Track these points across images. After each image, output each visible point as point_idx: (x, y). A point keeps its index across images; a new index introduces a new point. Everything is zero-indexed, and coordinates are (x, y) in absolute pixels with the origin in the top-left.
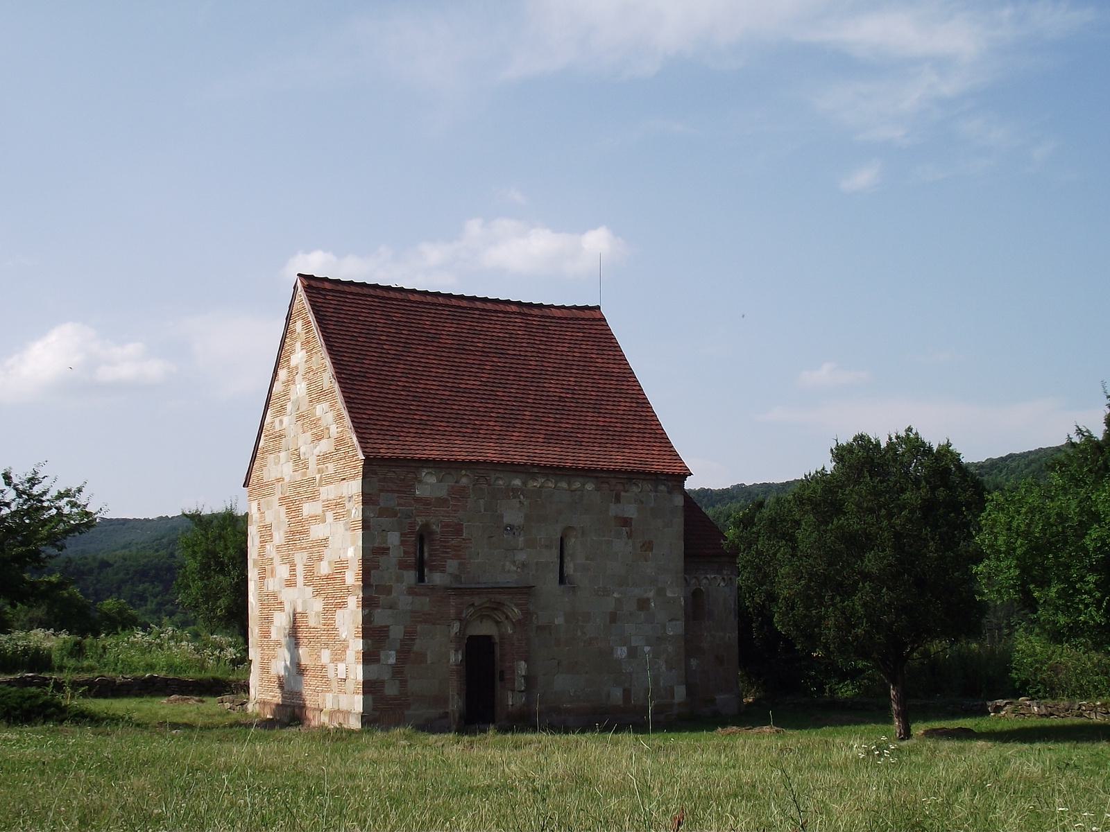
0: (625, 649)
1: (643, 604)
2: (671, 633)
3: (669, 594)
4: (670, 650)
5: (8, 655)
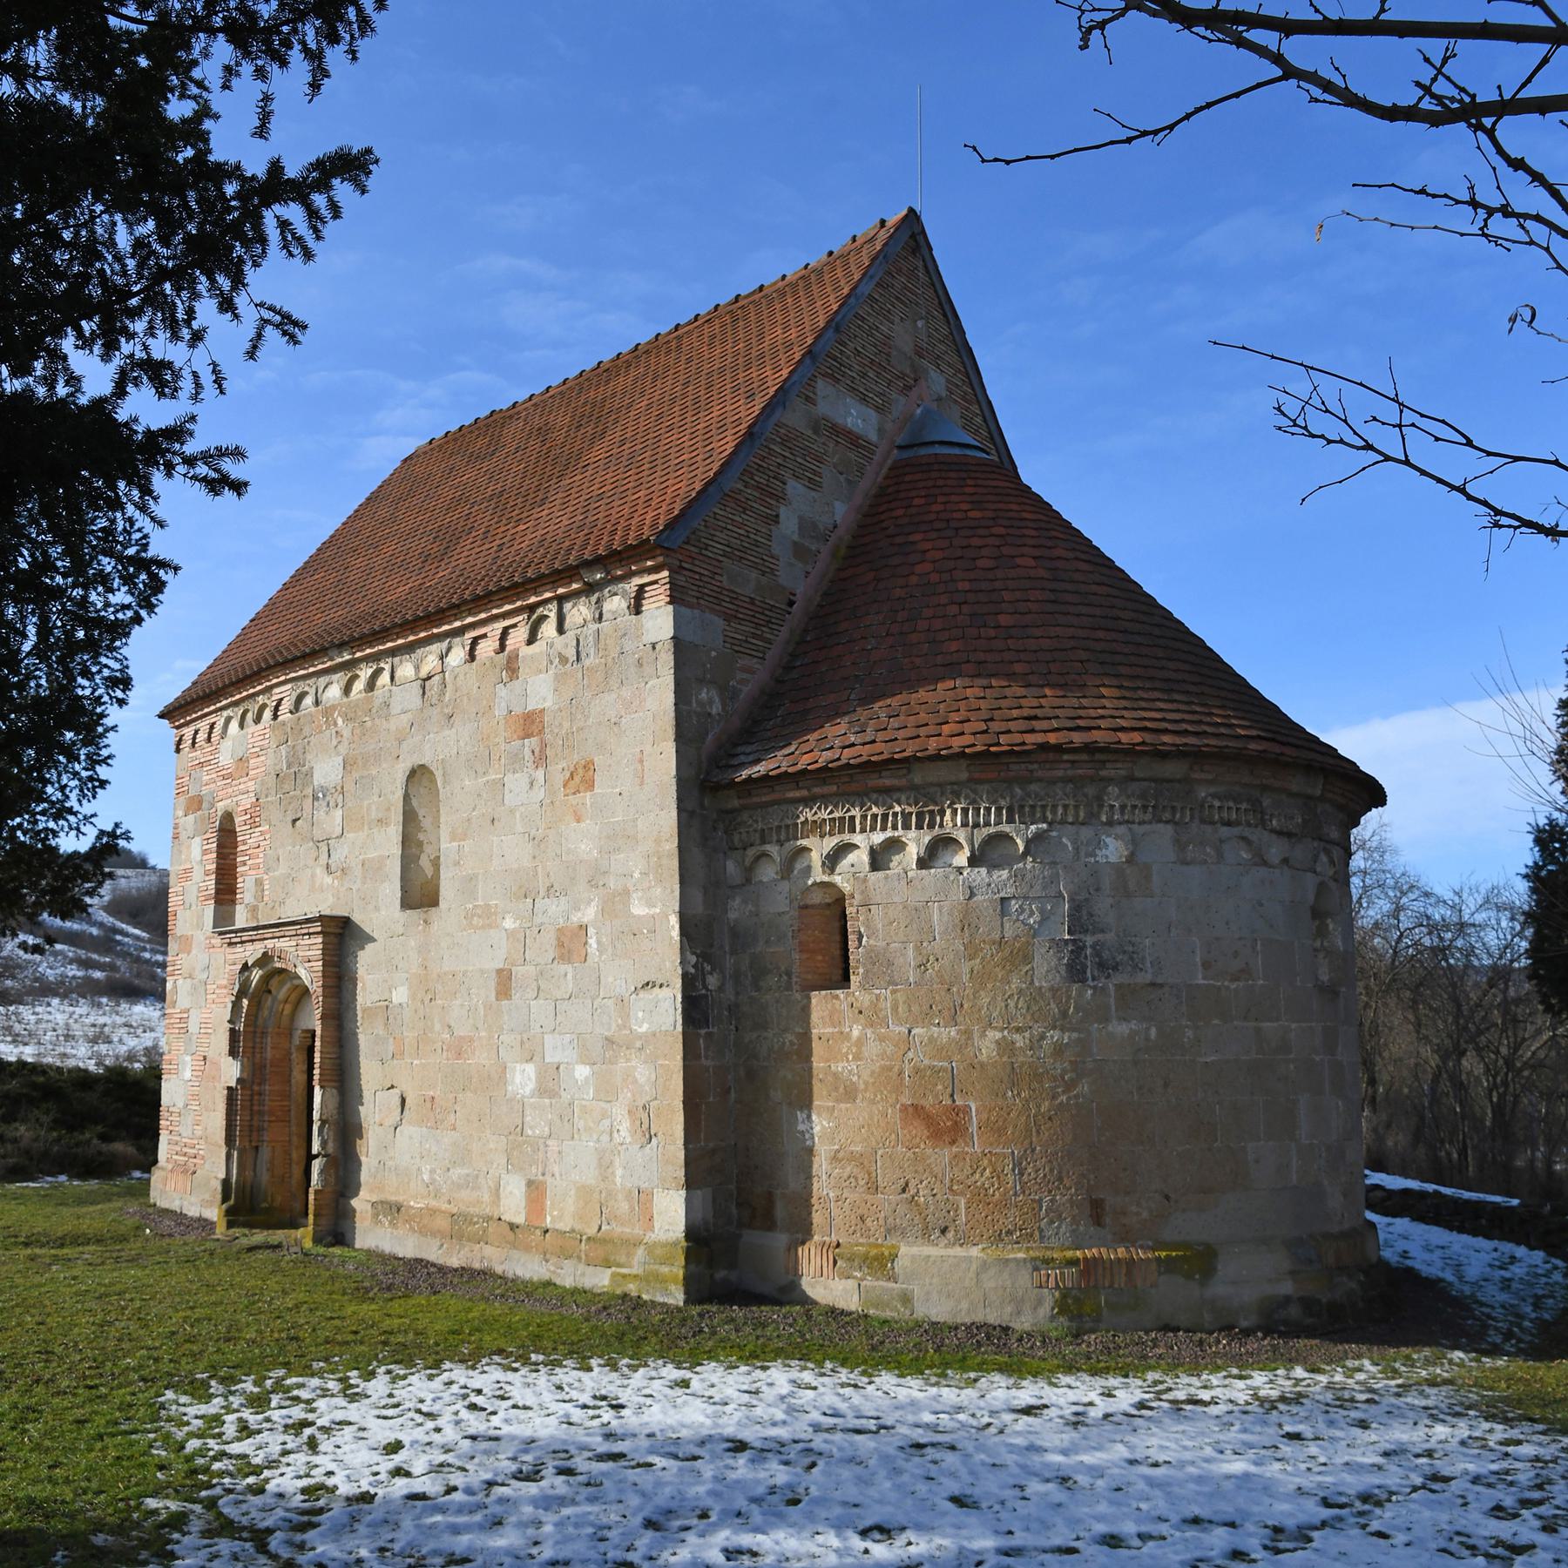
0: (530, 1069)
1: (570, 943)
2: (644, 1028)
3: (638, 909)
4: (642, 1080)
5: (113, 21)
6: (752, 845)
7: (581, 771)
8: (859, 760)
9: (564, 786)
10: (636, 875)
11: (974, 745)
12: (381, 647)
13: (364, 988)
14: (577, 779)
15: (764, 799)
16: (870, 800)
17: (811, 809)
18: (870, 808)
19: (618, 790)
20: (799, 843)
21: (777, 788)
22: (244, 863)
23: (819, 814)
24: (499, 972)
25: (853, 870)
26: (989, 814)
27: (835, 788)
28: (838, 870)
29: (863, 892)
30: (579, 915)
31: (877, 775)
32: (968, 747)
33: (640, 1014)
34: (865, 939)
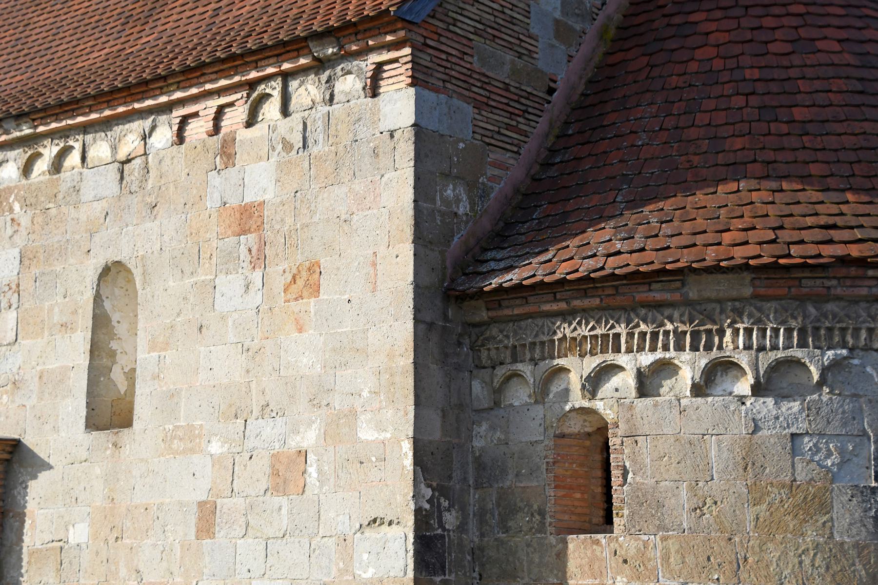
6: (502, 364)
7: (304, 274)
9: (285, 291)
10: (365, 394)
12: (70, 122)
13: (33, 526)
14: (300, 282)
15: (516, 312)
16: (637, 316)
17: (570, 324)
18: (638, 325)
19: (346, 297)
21: (531, 299)
23: (579, 331)
24: (201, 504)
25: (617, 395)
27: (597, 301)
28: (600, 395)
30: (298, 438)
31: (646, 288)
33: (365, 556)
34: (630, 475)
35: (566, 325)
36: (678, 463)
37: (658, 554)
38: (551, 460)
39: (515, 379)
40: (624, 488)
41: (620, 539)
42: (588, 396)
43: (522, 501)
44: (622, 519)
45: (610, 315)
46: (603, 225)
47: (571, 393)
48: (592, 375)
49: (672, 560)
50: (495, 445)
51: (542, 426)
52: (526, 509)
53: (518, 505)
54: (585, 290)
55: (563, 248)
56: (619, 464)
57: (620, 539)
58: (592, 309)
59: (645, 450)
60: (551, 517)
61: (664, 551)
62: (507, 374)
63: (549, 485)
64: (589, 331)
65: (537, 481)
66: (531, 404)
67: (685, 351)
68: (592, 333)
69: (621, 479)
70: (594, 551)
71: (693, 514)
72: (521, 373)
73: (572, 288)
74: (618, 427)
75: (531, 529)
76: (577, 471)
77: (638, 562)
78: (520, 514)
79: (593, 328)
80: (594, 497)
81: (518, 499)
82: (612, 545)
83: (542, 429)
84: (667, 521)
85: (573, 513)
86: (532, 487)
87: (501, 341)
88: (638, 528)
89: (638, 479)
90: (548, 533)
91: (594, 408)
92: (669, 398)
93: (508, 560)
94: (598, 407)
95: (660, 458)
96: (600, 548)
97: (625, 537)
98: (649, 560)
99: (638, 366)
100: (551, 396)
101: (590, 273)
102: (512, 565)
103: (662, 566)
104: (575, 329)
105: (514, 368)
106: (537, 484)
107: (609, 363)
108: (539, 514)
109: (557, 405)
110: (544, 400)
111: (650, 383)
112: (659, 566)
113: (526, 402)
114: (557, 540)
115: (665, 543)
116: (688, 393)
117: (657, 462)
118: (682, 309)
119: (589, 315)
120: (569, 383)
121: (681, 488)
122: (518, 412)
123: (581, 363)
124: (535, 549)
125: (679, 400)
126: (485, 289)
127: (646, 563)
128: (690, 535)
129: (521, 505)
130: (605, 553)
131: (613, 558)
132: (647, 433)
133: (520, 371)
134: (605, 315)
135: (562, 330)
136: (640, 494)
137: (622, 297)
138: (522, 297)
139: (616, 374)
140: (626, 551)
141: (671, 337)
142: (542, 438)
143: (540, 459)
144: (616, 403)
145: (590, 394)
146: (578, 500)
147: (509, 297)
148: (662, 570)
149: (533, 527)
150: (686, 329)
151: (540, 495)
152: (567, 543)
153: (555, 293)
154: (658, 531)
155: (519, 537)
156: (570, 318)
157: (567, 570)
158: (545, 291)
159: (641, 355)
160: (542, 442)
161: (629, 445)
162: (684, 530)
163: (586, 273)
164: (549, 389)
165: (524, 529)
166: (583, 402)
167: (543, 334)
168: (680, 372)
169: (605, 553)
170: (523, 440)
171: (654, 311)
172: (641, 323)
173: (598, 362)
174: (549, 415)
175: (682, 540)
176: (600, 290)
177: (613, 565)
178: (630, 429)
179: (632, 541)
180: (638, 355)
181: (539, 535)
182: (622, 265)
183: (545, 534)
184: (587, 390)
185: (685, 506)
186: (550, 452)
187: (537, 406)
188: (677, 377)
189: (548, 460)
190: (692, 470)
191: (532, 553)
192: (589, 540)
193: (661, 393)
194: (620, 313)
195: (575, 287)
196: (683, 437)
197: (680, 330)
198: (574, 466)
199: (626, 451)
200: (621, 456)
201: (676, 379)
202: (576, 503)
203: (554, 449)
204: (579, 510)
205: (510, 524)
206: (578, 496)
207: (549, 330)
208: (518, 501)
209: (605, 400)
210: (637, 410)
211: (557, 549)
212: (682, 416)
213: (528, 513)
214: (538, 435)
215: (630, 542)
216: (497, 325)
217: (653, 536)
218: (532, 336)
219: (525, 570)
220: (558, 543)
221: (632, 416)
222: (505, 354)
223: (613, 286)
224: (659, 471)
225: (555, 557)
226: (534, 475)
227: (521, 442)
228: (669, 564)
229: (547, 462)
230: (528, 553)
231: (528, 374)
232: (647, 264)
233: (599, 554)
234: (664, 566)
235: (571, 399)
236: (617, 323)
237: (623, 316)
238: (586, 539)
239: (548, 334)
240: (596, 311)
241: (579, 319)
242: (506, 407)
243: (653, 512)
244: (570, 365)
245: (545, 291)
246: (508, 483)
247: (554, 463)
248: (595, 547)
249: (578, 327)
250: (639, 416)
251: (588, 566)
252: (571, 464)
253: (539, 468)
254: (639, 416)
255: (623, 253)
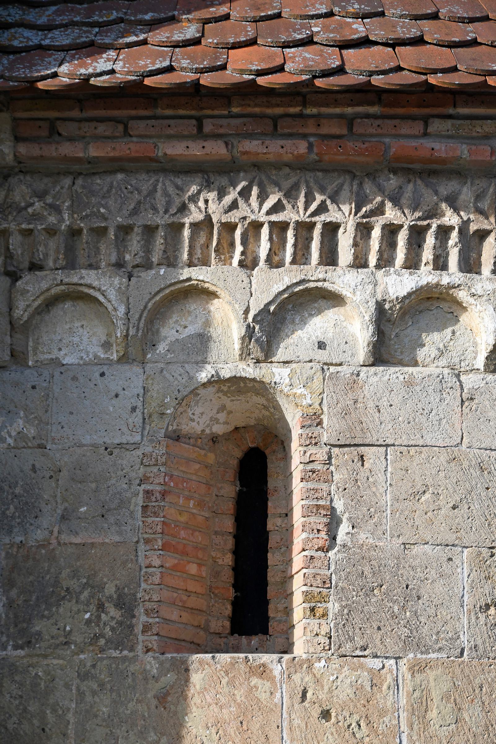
6: (35, 267)
8: (395, 80)
11: (455, 69)
15: (94, 152)
16: (381, 190)
17: (221, 196)
18: (379, 211)
20: (186, 273)
21: (138, 127)
22: (467, 316)
23: (243, 210)
25: (323, 356)
26: (393, 245)
27: (302, 147)
28: (281, 354)
29: (346, 413)
31: (418, 127)
32: (326, 74)
34: (343, 529)
35: (212, 196)
36: (454, 508)
37: (403, 701)
38: (158, 488)
39: (68, 305)
40: (331, 554)
41: (317, 665)
42: (257, 352)
43: (75, 574)
44: (322, 621)
45: (316, 182)
46: (223, 10)
47: (212, 345)
48: (272, 308)
49: (433, 714)
50: (9, 447)
51: (138, 412)
52: (86, 594)
53: (65, 584)
54: (275, 120)
55: (217, 20)
56: (321, 502)
57: (317, 665)
58: (278, 166)
59: (381, 477)
60: (147, 613)
61: (417, 694)
62: (53, 291)
63: (147, 541)
64: (268, 213)
65: (120, 533)
66: (109, 363)
67: (479, 273)
68: (274, 218)
69: (323, 535)
70: (252, 689)
71: (482, 617)
72: (91, 292)
73: (249, 110)
74: (320, 423)
75: (96, 638)
76: (193, 514)
77: (356, 717)
78: (68, 605)
79: (277, 208)
80: (217, 574)
81: (65, 573)
82: (297, 677)
83: (137, 418)
84: (425, 630)
85: (184, 608)
86: (103, 544)
87: (36, 217)
88: (360, 642)
89: (362, 536)
90: (140, 648)
91: (267, 380)
92: (438, 371)
93: (25, 710)
94: (277, 379)
95: (414, 494)
96: (268, 684)
97: (328, 660)
98: (383, 713)
99: (379, 298)
100: (162, 348)
101: (315, 77)
102: (36, 722)
103: (411, 727)
104: (234, 205)
105: (75, 279)
106: (117, 538)
107: (312, 285)
108: (118, 605)
109: (177, 369)
110: (144, 355)
111: (397, 336)
112: (404, 727)
113: (96, 357)
114: (161, 664)
115: (419, 677)
116: (480, 363)
117: (407, 503)
118: (482, 183)
119: (269, 178)
120: (208, 323)
121: (456, 560)
122: (75, 379)
123: (246, 280)
124: (102, 685)
125: (458, 376)
126: (40, 85)
127: (374, 718)
128: (475, 662)
129: (74, 584)
130: (278, 695)
131: (296, 706)
132: (390, 441)
133: (90, 286)
134: (307, 182)
135: (201, 204)
136: (367, 570)
137: (359, 144)
138: (116, 121)
139: (320, 312)
140: (330, 691)
141: (451, 242)
142: (138, 438)
143: (130, 483)
144: (319, 374)
145: (262, 350)
146: (193, 577)
147: (85, 115)
148: (410, 736)
149: (102, 636)
150: (489, 228)
151: (124, 563)
152: (187, 670)
153: (200, 121)
154: (405, 649)
155: (59, 657)
156: (224, 181)
157: (184, 732)
158: (181, 112)
159: (387, 274)
160: (136, 446)
161: (346, 463)
162: (463, 650)
163: (304, 77)
164: (158, 331)
165: (77, 638)
166: (242, 365)
167: (155, 209)
168: (464, 318)
169: (278, 695)
170: (87, 440)
171: (419, 182)
172: (389, 205)
173: (287, 281)
174: (155, 389)
175: (458, 671)
176: (311, 122)
177: (296, 722)
178: (350, 430)
179: (346, 671)
180: (380, 274)
181: (115, 654)
182: (386, 67)
183: (132, 649)
184: (257, 341)
185: (466, 598)
186: (155, 469)
187: (127, 367)
188: (456, 328)
189: (149, 487)
190: (482, 525)
191: (94, 693)
192: (242, 666)
193: (419, 360)
194: (340, 181)
195: (257, 110)
196: (466, 455)
197: (473, 227)
198: (192, 504)
199: (336, 477)
200: (324, 486)
201: (454, 333)
202: (192, 586)
203: (164, 464)
204: (193, 602)
205: (38, 626)
206: (193, 569)
207: (169, 204)
208: (64, 575)
209: (294, 365)
210: (367, 391)
211: (160, 685)
212: (465, 411)
213: (88, 604)
214: (125, 429)
215: (340, 672)
216: (28, 178)
217: (392, 662)
218: (126, 213)
219: (71, 731)
220: (163, 671)
221: (356, 402)
222: (46, 246)
223: (341, 116)
224: (411, 523)
225: (154, 702)
226: (112, 519)
227: (81, 446)
228: (426, 724)
229: (148, 493)
230: (81, 694)
231: (112, 294)
232: (444, 71)
233: (263, 696)
234: (415, 727)
235: (213, 356)
236: (334, 201)
237: (346, 187)
238: (233, 664)
239: (166, 212)
240: (287, 170)
241: (243, 184)
242: (40, 365)
243: (396, 608)
244: (221, 284)
245: (181, 112)
246: (40, 535)
247: (164, 494)
248: (255, 681)
249: (241, 202)
250: (371, 404)
251: (234, 724)
252: (188, 498)
253: (123, 503)
254: (371, 404)
255: (376, 43)
